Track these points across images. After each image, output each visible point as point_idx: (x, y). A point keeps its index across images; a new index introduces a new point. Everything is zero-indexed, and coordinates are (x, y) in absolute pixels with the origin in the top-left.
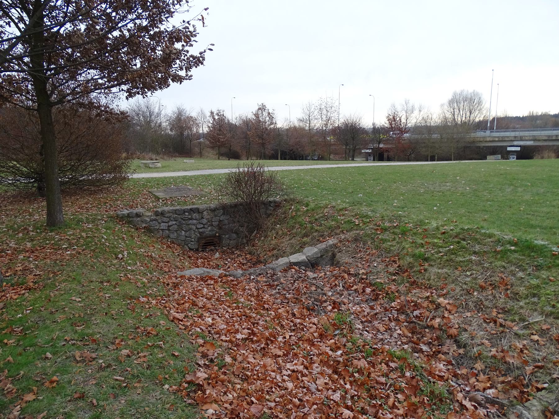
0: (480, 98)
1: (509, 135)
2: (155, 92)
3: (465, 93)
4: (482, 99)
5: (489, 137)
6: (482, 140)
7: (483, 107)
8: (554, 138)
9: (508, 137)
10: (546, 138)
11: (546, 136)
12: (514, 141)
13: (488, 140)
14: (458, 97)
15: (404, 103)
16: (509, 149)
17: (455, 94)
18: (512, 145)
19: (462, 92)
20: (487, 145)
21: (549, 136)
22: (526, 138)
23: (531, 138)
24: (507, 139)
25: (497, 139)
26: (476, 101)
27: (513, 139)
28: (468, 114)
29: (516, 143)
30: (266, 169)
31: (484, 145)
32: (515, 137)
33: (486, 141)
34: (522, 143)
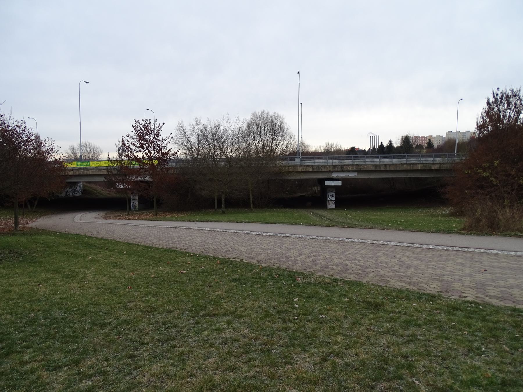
0: (281, 122)
1: (326, 164)
2: (93, 145)
3: (265, 116)
4: (284, 124)
5: (300, 166)
6: (291, 170)
7: (286, 133)
8: (382, 168)
9: (325, 166)
10: (373, 168)
11: (373, 165)
12: (333, 172)
13: (299, 170)
14: (258, 120)
15: (194, 123)
16: (327, 183)
17: (254, 116)
18: (331, 177)
19: (262, 113)
20: (298, 177)
21: (376, 166)
22: (349, 168)
23: (354, 168)
24: (324, 170)
25: (311, 169)
26: (277, 126)
27: (331, 169)
28: (270, 140)
29: (335, 175)
30: (290, 178)
31: (293, 177)
32: (334, 166)
33: (297, 172)
34: (343, 175)
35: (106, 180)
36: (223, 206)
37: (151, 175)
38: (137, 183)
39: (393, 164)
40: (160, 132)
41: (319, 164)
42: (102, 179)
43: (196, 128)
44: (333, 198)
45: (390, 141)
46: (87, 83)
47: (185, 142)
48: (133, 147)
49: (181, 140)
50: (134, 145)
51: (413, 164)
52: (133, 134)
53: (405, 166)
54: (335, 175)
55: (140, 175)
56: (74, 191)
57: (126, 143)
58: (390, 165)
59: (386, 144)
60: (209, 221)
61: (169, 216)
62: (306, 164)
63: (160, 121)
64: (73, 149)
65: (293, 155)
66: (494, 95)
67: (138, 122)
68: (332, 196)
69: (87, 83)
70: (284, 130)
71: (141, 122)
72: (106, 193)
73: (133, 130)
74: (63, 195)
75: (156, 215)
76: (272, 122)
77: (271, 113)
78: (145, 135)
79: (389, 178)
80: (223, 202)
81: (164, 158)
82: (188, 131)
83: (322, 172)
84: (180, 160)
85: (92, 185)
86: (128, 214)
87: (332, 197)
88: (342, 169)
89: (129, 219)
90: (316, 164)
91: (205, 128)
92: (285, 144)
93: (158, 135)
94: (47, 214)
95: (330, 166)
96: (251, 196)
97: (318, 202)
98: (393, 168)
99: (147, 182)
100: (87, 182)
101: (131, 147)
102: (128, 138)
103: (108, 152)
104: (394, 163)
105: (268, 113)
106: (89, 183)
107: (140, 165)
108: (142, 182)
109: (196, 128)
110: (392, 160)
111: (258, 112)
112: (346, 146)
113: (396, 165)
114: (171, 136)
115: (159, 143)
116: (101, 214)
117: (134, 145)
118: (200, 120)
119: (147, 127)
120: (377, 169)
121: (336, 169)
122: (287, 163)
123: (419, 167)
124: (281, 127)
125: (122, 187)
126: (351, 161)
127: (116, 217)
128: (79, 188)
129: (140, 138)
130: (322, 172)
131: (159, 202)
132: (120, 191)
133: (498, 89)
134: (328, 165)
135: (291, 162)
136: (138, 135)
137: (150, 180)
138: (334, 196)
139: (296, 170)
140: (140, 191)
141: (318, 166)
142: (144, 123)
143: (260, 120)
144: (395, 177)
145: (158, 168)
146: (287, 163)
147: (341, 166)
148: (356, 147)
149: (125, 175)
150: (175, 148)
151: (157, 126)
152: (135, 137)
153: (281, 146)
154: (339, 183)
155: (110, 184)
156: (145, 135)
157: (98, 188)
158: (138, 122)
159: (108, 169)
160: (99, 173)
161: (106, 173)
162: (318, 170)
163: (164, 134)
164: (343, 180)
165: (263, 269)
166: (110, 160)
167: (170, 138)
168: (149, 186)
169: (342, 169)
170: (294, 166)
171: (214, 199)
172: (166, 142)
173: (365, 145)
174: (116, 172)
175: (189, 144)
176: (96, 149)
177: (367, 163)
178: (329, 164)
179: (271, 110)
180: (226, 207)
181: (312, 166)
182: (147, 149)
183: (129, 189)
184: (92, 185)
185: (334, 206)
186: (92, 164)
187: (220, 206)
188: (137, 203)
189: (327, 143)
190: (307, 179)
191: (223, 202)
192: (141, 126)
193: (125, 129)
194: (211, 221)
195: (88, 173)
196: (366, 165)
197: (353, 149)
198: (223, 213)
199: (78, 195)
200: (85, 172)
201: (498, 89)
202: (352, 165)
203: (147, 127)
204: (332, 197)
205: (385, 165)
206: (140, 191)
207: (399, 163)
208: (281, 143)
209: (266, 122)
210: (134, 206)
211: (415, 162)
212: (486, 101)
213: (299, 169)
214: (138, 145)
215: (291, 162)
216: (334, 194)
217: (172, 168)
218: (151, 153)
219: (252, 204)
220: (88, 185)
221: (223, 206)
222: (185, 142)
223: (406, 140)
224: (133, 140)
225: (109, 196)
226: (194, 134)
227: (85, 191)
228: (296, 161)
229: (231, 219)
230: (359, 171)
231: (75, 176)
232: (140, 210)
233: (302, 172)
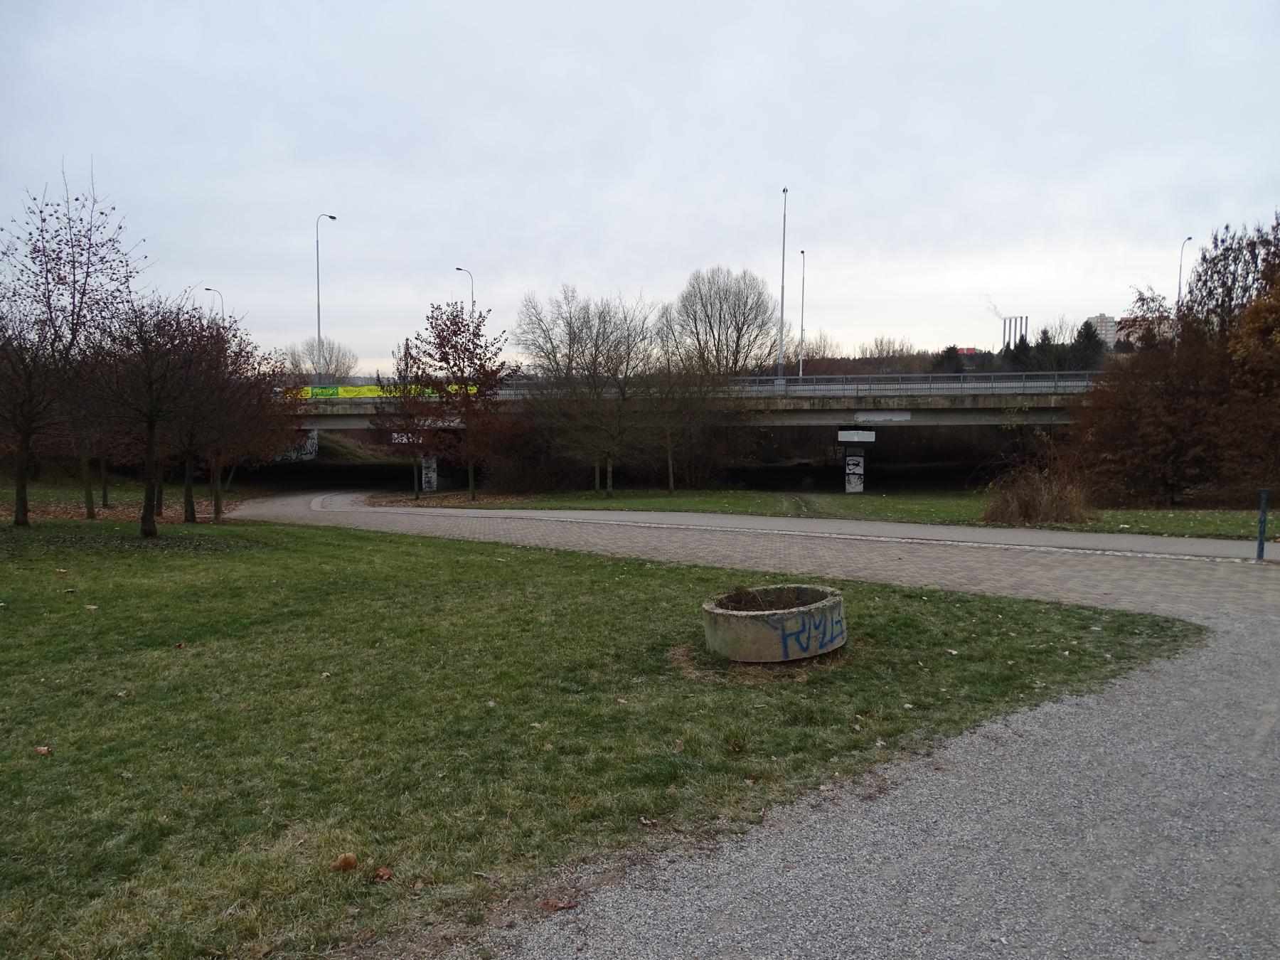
0: (760, 294)
1: (840, 393)
4: (765, 297)
5: (784, 397)
6: (762, 407)
8: (968, 404)
9: (838, 399)
10: (947, 404)
11: (946, 397)
13: (781, 407)
15: (561, 298)
16: (844, 436)
17: (697, 277)
18: (852, 423)
19: (715, 273)
21: (953, 398)
22: (892, 404)
23: (904, 403)
24: (835, 406)
25: (806, 406)
26: (750, 302)
27: (852, 406)
29: (861, 418)
30: (757, 424)
31: (767, 422)
32: (859, 399)
35: (372, 427)
36: (609, 482)
37: (465, 417)
38: (436, 432)
39: (993, 395)
40: (482, 328)
41: (826, 393)
42: (365, 424)
43: (565, 308)
44: (860, 470)
45: (1045, 333)
46: (333, 218)
47: (541, 341)
48: (428, 360)
49: (530, 336)
50: (430, 355)
51: (1038, 395)
52: (429, 335)
53: (1019, 398)
54: (861, 418)
55: (441, 416)
56: (300, 449)
57: (414, 352)
58: (985, 396)
59: (1033, 340)
60: (570, 509)
61: (499, 501)
62: (799, 394)
63: (481, 308)
64: (293, 354)
65: (788, 370)
66: (1216, 239)
67: (439, 308)
68: (857, 465)
69: (333, 218)
70: (765, 312)
71: (444, 308)
72: (368, 454)
73: (428, 326)
74: (278, 459)
75: (473, 499)
76: (738, 294)
77: (736, 272)
78: (452, 332)
79: (970, 426)
80: (610, 475)
81: (488, 379)
82: (547, 314)
83: (831, 411)
84: (528, 381)
85: (338, 437)
86: (417, 498)
87: (855, 467)
88: (877, 405)
89: (419, 506)
90: (818, 393)
91: (586, 309)
92: (769, 344)
93: (476, 335)
94: (254, 497)
95: (850, 397)
96: (670, 462)
97: (829, 479)
98: (991, 404)
99: (454, 432)
100: (327, 431)
101: (424, 360)
102: (418, 343)
103: (374, 360)
104: (997, 391)
105: (729, 273)
106: (331, 431)
107: (441, 397)
108: (444, 430)
109: (565, 308)
110: (989, 385)
111: (705, 271)
112: (935, 345)
113: (999, 396)
114: (505, 336)
115: (478, 351)
116: (362, 497)
117: (430, 355)
118: (573, 291)
119: (456, 322)
120: (955, 407)
121: (863, 406)
122: (753, 391)
123: (1053, 402)
124: (760, 306)
125: (405, 440)
126: (897, 386)
127: (392, 504)
128: (311, 445)
129: (442, 341)
130: (831, 411)
131: (478, 472)
132: (400, 449)
133: (1227, 228)
134: (845, 397)
135: (765, 390)
136: (439, 336)
137: (462, 426)
138: (862, 464)
139: (773, 408)
140: (440, 450)
141: (823, 398)
142: (449, 310)
143: (710, 290)
144: (935, 423)
145: (476, 402)
146: (753, 391)
147: (875, 397)
148: (963, 344)
149: (411, 416)
150: (513, 355)
151: (476, 315)
152: (432, 340)
153: (758, 350)
154: (870, 437)
155: (379, 436)
156: (452, 332)
157: (350, 443)
158: (439, 308)
159: (378, 405)
160: (356, 412)
161: (371, 410)
162: (822, 407)
163: (489, 332)
164: (878, 429)
165: (620, 560)
166: (379, 381)
167: (503, 340)
168: (460, 440)
169: (877, 405)
170: (769, 398)
171: (593, 469)
172: (493, 349)
173: (993, 344)
174: (391, 410)
175: (549, 345)
176: (344, 355)
177: (934, 392)
178: (847, 393)
179: (734, 267)
180: (614, 486)
181: (810, 398)
182: (455, 365)
183: (418, 445)
184: (338, 437)
185: (860, 488)
186: (343, 393)
187: (603, 485)
188: (434, 476)
189: (879, 338)
190: (809, 427)
191: (610, 475)
192: (445, 317)
193: (418, 329)
194: (575, 509)
195: (336, 410)
196: (930, 396)
197: (952, 353)
198: (609, 496)
199: (308, 457)
200: (329, 410)
201: (1227, 228)
202: (900, 396)
203: (456, 322)
204: (855, 467)
205: (975, 397)
206: (440, 450)
207: (1010, 392)
208: (759, 342)
209: (724, 294)
210: (429, 482)
211: (1045, 391)
212: (1200, 256)
213: (781, 405)
214: (437, 357)
215: (765, 390)
216: (861, 460)
217: (505, 403)
218: (463, 372)
219: (672, 481)
220: (327, 435)
221: (609, 482)
222: (541, 341)
223: (1088, 332)
224: (428, 347)
225: (373, 460)
226: (560, 322)
227: (322, 450)
228: (776, 388)
229: (622, 505)
230: (915, 411)
231: (307, 417)
232: (439, 490)
233: (785, 411)
